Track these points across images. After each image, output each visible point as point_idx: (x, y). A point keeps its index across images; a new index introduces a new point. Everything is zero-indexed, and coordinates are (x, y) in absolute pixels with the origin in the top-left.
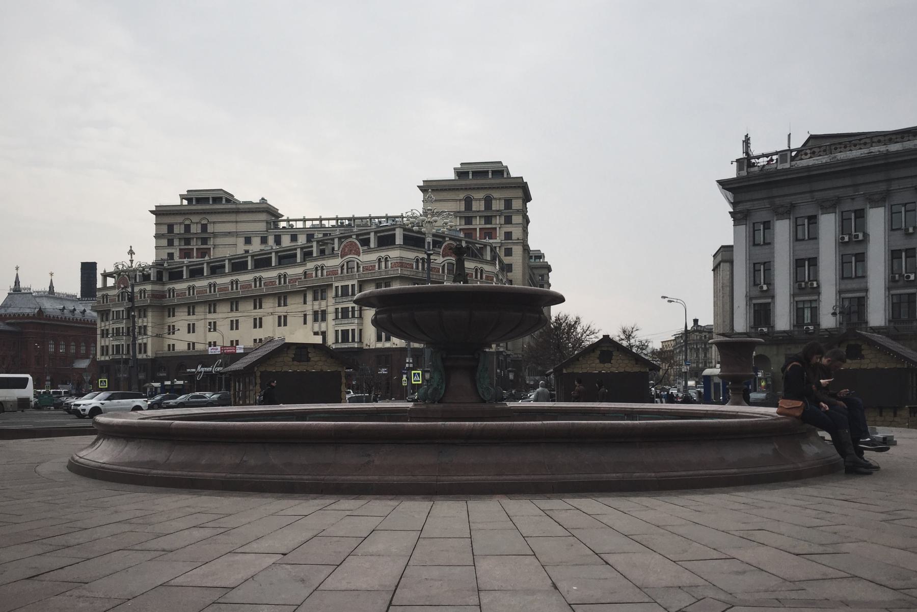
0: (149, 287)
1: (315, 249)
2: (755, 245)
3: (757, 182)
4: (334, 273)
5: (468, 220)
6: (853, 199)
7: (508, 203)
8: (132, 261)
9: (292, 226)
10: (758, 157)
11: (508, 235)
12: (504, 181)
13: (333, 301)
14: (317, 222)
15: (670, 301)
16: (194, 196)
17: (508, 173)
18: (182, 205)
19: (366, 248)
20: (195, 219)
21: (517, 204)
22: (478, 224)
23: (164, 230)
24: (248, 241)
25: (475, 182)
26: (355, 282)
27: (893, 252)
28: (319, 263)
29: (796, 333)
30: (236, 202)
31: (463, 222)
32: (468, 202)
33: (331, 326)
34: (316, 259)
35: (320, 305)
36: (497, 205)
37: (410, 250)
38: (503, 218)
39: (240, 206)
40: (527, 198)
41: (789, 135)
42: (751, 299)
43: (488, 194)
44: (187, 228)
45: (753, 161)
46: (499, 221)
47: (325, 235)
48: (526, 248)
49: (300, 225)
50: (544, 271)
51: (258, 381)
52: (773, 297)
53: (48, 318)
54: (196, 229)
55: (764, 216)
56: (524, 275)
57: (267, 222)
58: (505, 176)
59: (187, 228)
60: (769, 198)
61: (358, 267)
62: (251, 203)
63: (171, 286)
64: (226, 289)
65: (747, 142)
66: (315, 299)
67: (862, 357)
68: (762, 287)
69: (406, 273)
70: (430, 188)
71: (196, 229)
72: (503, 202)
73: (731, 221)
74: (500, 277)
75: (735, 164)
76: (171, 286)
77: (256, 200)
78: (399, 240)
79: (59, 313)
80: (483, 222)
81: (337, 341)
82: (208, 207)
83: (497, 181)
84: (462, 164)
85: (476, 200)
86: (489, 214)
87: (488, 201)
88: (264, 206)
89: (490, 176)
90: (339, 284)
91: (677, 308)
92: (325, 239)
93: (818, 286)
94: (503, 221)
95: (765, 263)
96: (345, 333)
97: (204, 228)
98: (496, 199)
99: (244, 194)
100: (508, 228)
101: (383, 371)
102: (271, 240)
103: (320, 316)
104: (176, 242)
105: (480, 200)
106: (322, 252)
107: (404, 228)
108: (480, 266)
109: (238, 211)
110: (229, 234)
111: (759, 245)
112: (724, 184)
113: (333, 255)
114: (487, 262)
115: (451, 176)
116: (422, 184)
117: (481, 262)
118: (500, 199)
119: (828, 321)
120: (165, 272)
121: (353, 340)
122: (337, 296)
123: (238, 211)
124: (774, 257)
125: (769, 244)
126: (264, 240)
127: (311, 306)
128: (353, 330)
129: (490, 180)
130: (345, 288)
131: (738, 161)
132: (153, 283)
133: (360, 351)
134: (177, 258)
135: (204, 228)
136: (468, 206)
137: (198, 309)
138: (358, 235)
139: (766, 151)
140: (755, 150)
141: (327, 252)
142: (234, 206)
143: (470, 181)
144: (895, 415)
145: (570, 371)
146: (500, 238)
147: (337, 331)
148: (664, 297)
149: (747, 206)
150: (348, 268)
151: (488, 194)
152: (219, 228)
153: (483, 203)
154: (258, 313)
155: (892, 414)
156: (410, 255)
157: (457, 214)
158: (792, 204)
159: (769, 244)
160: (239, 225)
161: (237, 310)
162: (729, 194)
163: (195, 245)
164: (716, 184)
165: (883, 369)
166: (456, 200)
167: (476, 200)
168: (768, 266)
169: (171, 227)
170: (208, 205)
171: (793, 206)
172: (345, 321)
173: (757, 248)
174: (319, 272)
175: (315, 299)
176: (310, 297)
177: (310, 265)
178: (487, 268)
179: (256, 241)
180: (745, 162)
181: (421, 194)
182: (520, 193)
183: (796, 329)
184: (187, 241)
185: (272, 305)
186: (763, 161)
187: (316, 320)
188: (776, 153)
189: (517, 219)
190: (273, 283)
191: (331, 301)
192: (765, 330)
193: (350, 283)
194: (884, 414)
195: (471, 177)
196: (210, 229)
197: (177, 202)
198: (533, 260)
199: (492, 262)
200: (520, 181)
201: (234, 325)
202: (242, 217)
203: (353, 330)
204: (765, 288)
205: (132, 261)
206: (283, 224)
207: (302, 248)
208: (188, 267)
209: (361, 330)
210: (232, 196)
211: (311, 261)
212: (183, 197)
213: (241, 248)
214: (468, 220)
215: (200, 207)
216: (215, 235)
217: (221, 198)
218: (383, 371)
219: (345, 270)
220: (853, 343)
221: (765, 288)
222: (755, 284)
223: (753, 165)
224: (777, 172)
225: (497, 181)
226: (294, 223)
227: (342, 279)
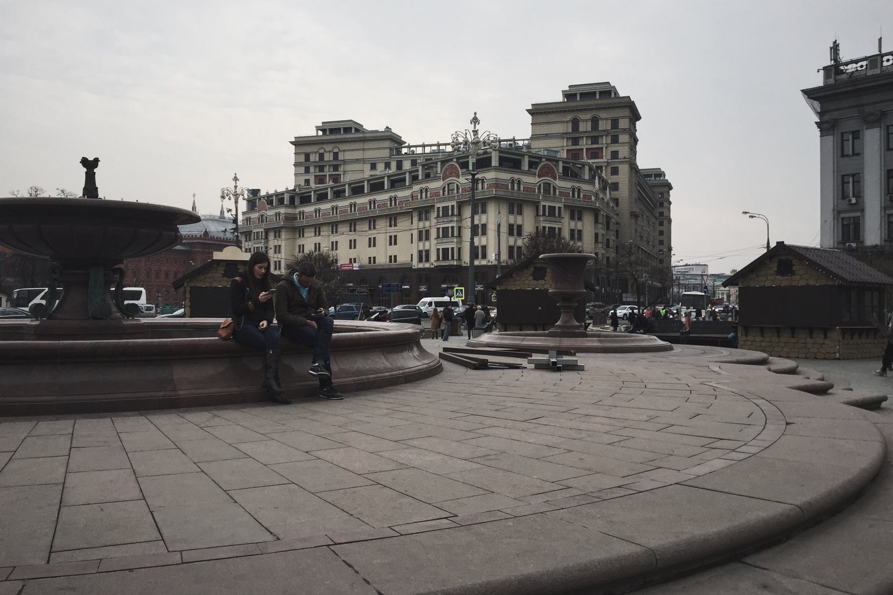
0: (282, 211)
1: (420, 173)
2: (843, 156)
3: (844, 90)
4: (437, 194)
5: (575, 141)
7: (615, 122)
8: (236, 187)
9: (413, 152)
10: (847, 64)
12: (611, 101)
13: (435, 221)
14: (435, 148)
15: (752, 217)
17: (616, 93)
18: (317, 136)
19: (464, 170)
20: (329, 148)
21: (624, 124)
22: (585, 144)
23: (302, 158)
24: (373, 167)
25: (583, 103)
26: (454, 203)
28: (424, 186)
29: (887, 248)
30: (365, 132)
31: (570, 143)
32: (575, 123)
33: (433, 245)
34: (421, 183)
36: (604, 125)
37: (505, 171)
40: (635, 116)
41: (880, 40)
42: (839, 212)
43: (596, 115)
44: (321, 156)
45: (842, 68)
46: (605, 140)
47: (426, 160)
48: (633, 167)
49: (419, 150)
50: (666, 189)
51: (188, 296)
52: (863, 210)
53: (212, 239)
54: (328, 157)
55: (851, 125)
56: (631, 192)
57: (391, 149)
58: (613, 96)
59: (321, 156)
60: (856, 106)
61: (458, 189)
62: (377, 131)
63: (301, 209)
64: (346, 211)
65: (835, 48)
66: (420, 220)
67: (793, 273)
68: (850, 200)
69: (501, 193)
70: (538, 112)
71: (328, 157)
73: (817, 132)
74: (601, 196)
75: (822, 72)
76: (301, 209)
77: (382, 129)
78: (495, 162)
79: (222, 235)
80: (590, 142)
81: (438, 259)
82: (339, 137)
83: (605, 101)
84: (570, 86)
85: (583, 121)
86: (596, 134)
87: (595, 121)
88: (388, 134)
89: (598, 97)
90: (441, 205)
91: (759, 223)
94: (609, 141)
95: (853, 175)
96: (445, 251)
97: (336, 155)
98: (602, 119)
99: (372, 123)
100: (614, 148)
102: (394, 165)
103: (576, 236)
104: (312, 169)
105: (587, 120)
106: (427, 176)
107: (501, 150)
108: (577, 185)
110: (357, 161)
111: (848, 156)
112: (810, 94)
113: (436, 178)
115: (559, 98)
116: (293, 140)
117: (579, 182)
118: (606, 119)
120: (298, 197)
121: (453, 258)
122: (438, 216)
123: (364, 140)
124: (863, 169)
125: (858, 154)
126: (388, 165)
127: (417, 224)
128: (452, 249)
129: (598, 100)
130: (445, 209)
131: (825, 68)
132: (286, 206)
133: (459, 268)
134: (313, 185)
135: (336, 155)
136: (575, 127)
137: (323, 229)
138: (458, 159)
139: (854, 58)
140: (844, 56)
141: (432, 176)
142: (361, 135)
143: (578, 102)
144: (826, 338)
145: (503, 288)
146: (606, 156)
147: (438, 250)
148: (746, 213)
149: (835, 115)
150: (449, 190)
151: (596, 115)
152: (349, 156)
153: (589, 124)
154: (372, 233)
155: (822, 336)
156: (505, 176)
158: (882, 112)
159: (858, 154)
160: (346, 153)
161: (374, 228)
162: (817, 104)
163: (328, 171)
164: (801, 94)
165: (814, 286)
166: (563, 122)
167: (583, 121)
168: (857, 178)
169: (307, 156)
170: (341, 134)
171: (884, 114)
172: (445, 240)
173: (846, 158)
174: (424, 194)
175: (420, 220)
176: (415, 219)
177: (416, 188)
179: (381, 167)
180: (834, 70)
181: (529, 118)
182: (626, 112)
183: (887, 244)
184: (321, 169)
185: (384, 225)
186: (851, 68)
187: (420, 239)
188: (866, 59)
189: (624, 138)
190: (385, 205)
191: (434, 221)
192: (854, 245)
193: (449, 204)
194: (814, 335)
195: (578, 99)
196: (341, 157)
198: (653, 178)
199: (591, 181)
200: (628, 100)
201: (372, 243)
202: (368, 145)
203: (452, 249)
204: (854, 201)
205: (236, 187)
206: (404, 151)
208: (315, 191)
209: (459, 249)
210: (362, 126)
211: (416, 184)
212: (318, 128)
213: (368, 173)
214: (575, 141)
215: (333, 137)
216: (345, 162)
217: (351, 128)
219: (446, 193)
220: (783, 258)
221: (854, 201)
222: (844, 196)
223: (842, 72)
224: (867, 78)
225: (605, 101)
226: (414, 149)
227: (444, 200)
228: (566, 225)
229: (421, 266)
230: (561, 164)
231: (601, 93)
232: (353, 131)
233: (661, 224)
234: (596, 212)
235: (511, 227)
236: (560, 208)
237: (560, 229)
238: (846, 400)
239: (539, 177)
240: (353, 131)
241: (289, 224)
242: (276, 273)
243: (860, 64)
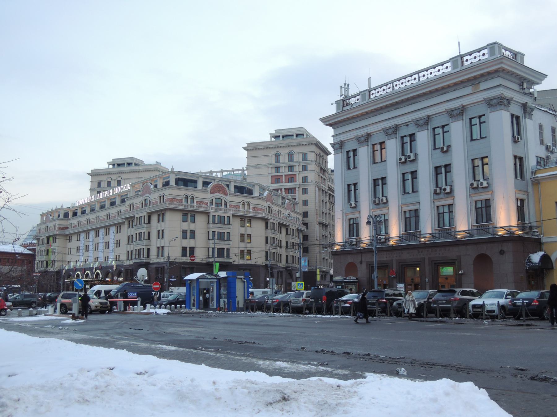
6: (407, 125)
11: (305, 179)
16: (116, 163)
20: (114, 177)
23: (96, 185)
26: (145, 214)
27: (436, 168)
32: (277, 156)
36: (297, 158)
38: (301, 167)
62: (151, 165)
70: (251, 148)
75: (335, 105)
78: (172, 183)
84: (276, 131)
87: (291, 155)
93: (387, 201)
100: (305, 174)
101: (268, 279)
105: (285, 155)
108: (246, 200)
116: (246, 146)
118: (299, 153)
119: (505, 218)
131: (337, 102)
136: (277, 161)
153: (287, 156)
157: (269, 166)
169: (99, 184)
170: (123, 166)
172: (140, 242)
180: (343, 103)
181: (245, 152)
197: (105, 166)
212: (109, 164)
218: (268, 279)
223: (347, 104)
228: (235, 229)
229: (158, 261)
232: (133, 164)
235: (242, 235)
237: (228, 233)
239: (211, 193)
240: (133, 164)
241: (62, 233)
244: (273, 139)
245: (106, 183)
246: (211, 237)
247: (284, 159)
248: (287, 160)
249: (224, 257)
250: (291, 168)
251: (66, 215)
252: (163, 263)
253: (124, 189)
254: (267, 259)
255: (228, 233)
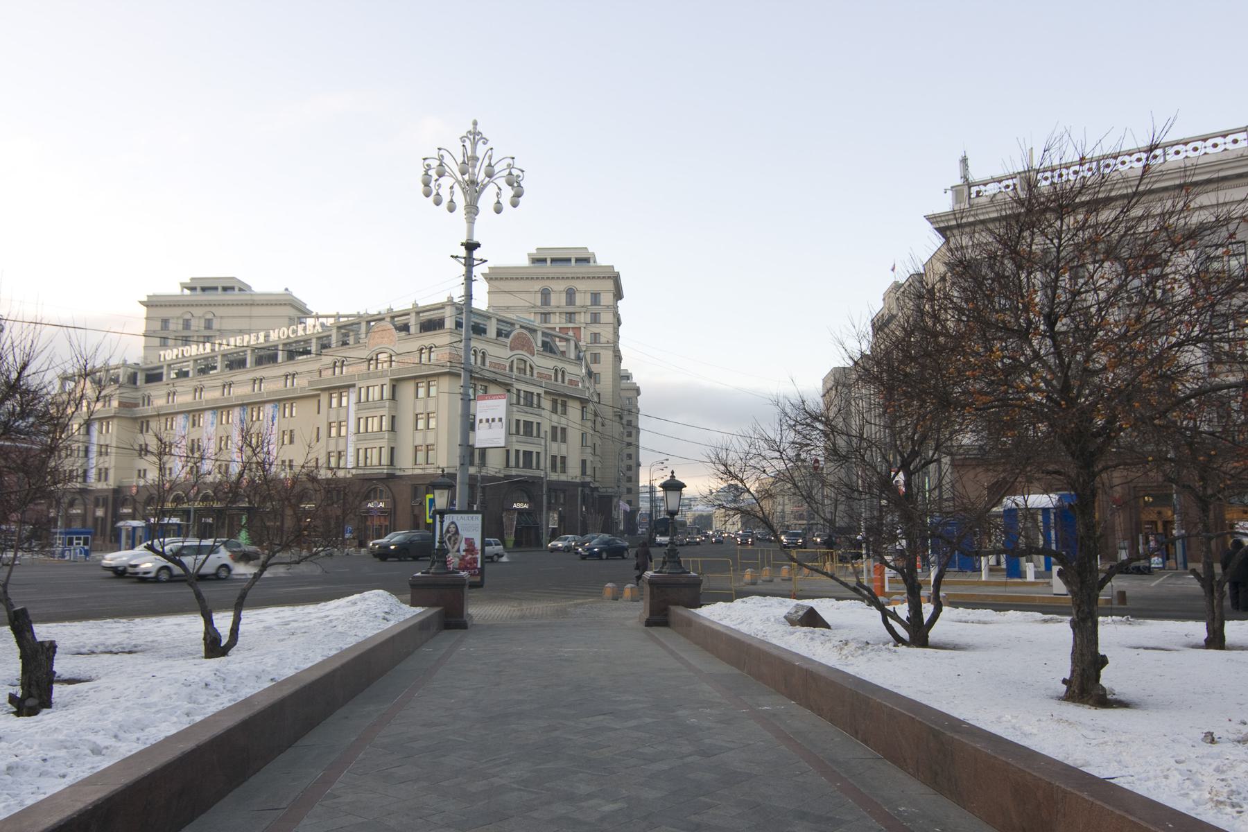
5: (546, 316)
7: (596, 297)
11: (596, 337)
20: (198, 312)
21: (607, 299)
23: (157, 326)
32: (546, 294)
35: (559, 449)
36: (581, 299)
39: (255, 298)
40: (619, 295)
72: (589, 296)
75: (950, 193)
77: (281, 290)
87: (571, 293)
92: (349, 330)
97: (208, 325)
100: (595, 329)
105: (560, 292)
109: (252, 304)
114: (570, 362)
115: (525, 262)
116: (145, 299)
123: (252, 304)
135: (208, 325)
139: (998, 173)
152: (228, 325)
153: (564, 295)
169: (165, 322)
170: (216, 294)
177: (327, 360)
178: (570, 368)
181: (143, 311)
182: (610, 285)
186: (992, 189)
189: (606, 317)
196: (216, 325)
207: (318, 338)
209: (392, 449)
214: (546, 316)
230: (539, 334)
231: (577, 260)
233: (630, 435)
234: (584, 402)
236: (539, 395)
237: (538, 424)
238: (1055, 694)
239: (512, 349)
242: (101, 486)
243: (1005, 183)
244: (187, 292)
245: (181, 321)
246: (513, 430)
247: (558, 300)
248: (563, 302)
249: (531, 468)
250: (570, 316)
251: (133, 379)
252: (105, 490)
253: (301, 332)
254: (584, 473)
255: (538, 424)
